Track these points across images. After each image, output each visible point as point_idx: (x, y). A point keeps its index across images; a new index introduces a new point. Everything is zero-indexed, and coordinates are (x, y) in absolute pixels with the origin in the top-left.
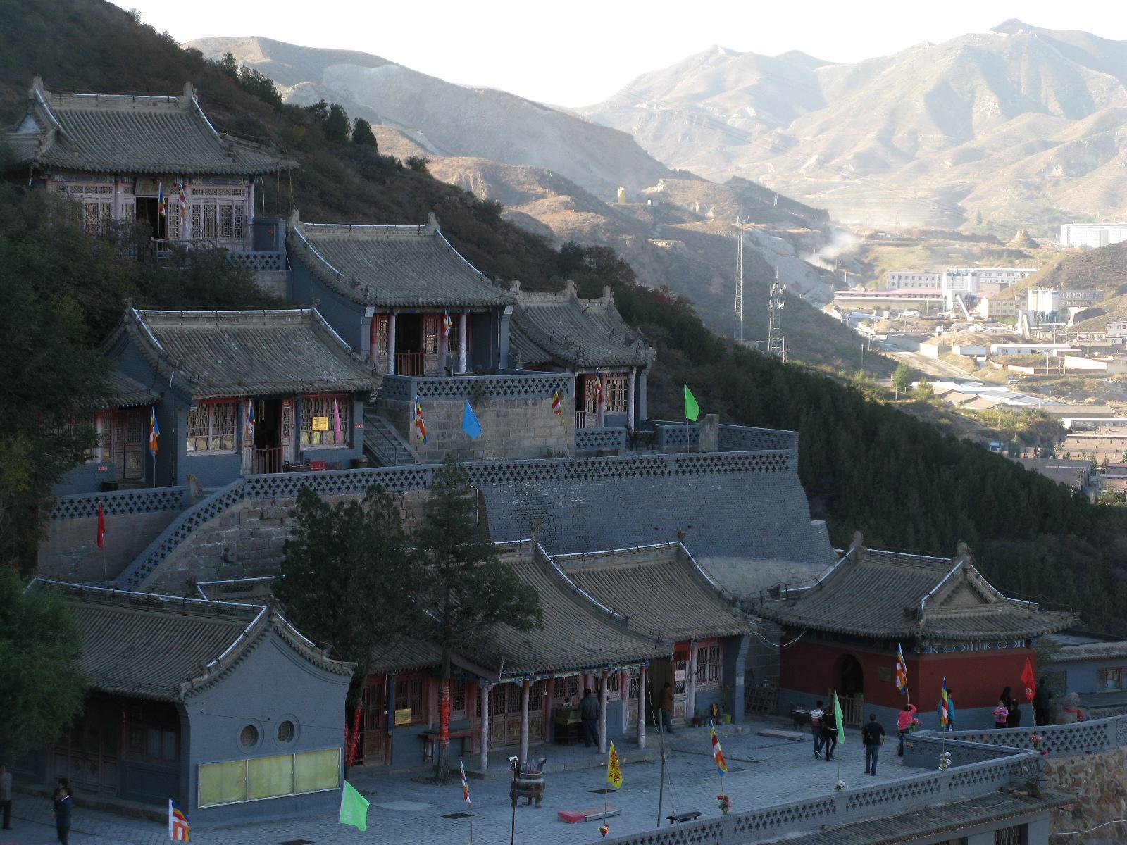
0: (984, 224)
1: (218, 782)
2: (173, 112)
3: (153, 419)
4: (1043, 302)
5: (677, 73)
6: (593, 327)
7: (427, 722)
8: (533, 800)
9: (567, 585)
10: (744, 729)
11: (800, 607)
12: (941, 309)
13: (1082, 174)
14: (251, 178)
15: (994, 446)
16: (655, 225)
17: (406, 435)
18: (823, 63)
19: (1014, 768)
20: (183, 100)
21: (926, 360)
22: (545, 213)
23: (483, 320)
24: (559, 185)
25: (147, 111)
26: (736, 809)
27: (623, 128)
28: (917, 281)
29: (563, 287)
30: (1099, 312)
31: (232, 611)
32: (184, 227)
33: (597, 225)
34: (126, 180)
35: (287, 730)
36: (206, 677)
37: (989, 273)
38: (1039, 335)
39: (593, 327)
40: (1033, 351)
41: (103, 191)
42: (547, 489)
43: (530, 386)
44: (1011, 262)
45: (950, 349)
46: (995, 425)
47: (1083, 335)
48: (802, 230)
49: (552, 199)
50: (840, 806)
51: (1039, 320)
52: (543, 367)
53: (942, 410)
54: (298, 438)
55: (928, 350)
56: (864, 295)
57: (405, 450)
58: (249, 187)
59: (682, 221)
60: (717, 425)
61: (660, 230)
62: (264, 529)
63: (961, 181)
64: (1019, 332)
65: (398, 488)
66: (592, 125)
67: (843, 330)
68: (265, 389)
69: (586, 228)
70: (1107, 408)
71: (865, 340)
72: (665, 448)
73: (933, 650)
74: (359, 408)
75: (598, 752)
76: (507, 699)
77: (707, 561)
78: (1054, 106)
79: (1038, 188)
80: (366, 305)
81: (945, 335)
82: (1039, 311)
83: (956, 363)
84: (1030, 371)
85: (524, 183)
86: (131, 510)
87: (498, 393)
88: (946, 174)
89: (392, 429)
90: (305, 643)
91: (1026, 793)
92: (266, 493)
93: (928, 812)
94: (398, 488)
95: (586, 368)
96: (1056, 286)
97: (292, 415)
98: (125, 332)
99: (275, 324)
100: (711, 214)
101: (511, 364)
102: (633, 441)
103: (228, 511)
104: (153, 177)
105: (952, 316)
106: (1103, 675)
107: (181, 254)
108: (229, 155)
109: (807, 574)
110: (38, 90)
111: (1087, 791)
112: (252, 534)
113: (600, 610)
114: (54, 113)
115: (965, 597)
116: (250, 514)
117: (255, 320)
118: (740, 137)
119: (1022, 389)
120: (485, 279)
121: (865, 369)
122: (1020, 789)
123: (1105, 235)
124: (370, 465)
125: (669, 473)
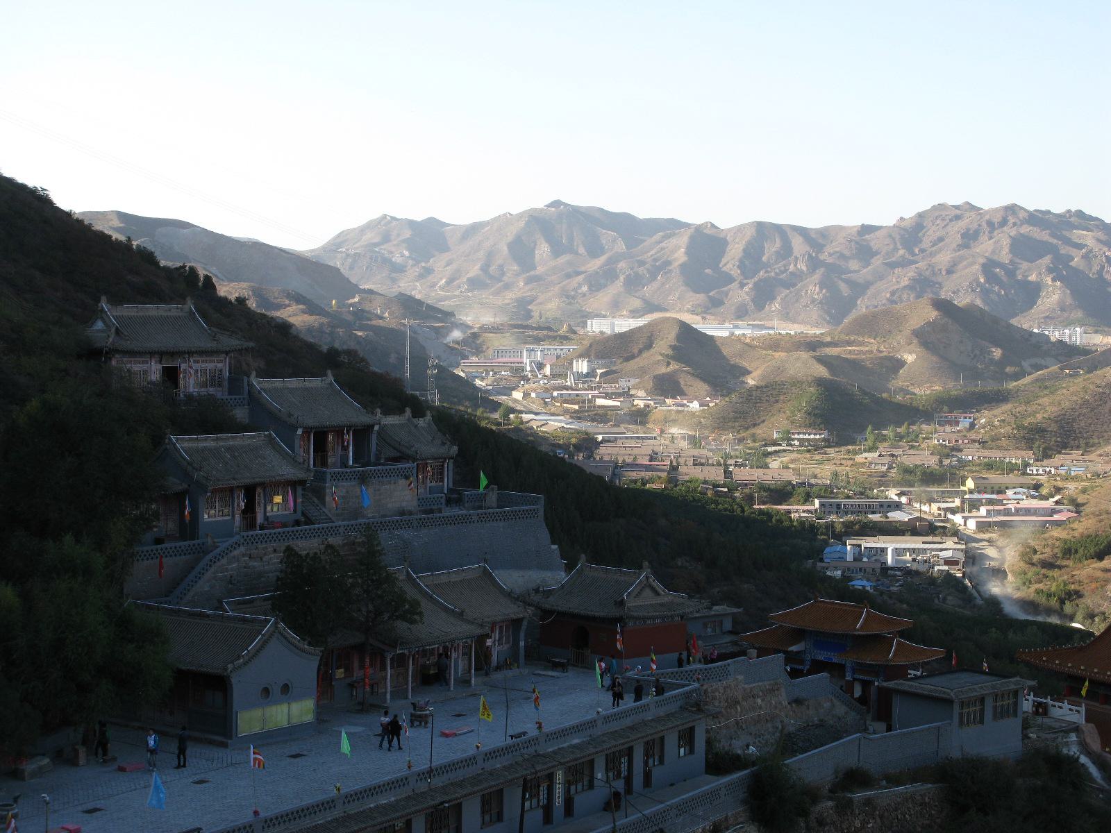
0: (543, 319)
1: (249, 720)
2: (181, 314)
3: (187, 502)
4: (582, 366)
5: (363, 230)
6: (423, 437)
7: (353, 676)
8: (423, 723)
9: (427, 593)
10: (525, 671)
11: (551, 599)
12: (523, 370)
13: (598, 290)
14: (227, 353)
15: (560, 453)
16: (355, 322)
17: (324, 503)
18: (449, 225)
19: (688, 695)
20: (186, 307)
21: (516, 401)
22: (290, 316)
23: (362, 433)
24: (299, 299)
25: (165, 314)
26: (546, 729)
27: (331, 264)
28: (508, 354)
29: (404, 412)
30: (615, 372)
31: (253, 621)
32: (189, 382)
33: (323, 323)
34: (156, 356)
35: (286, 689)
36: (242, 660)
37: (549, 349)
38: (580, 386)
39: (423, 437)
40: (577, 395)
41: (143, 362)
42: (407, 534)
43: (392, 473)
44: (561, 342)
45: (530, 394)
46: (559, 440)
47: (605, 386)
48: (440, 325)
49: (294, 308)
50: (599, 723)
51: (580, 377)
52: (395, 460)
53: (529, 431)
54: (265, 508)
55: (517, 395)
56: (478, 363)
57: (324, 512)
58: (225, 358)
59: (371, 320)
60: (496, 491)
61: (357, 325)
62: (252, 563)
63: (530, 294)
64: (569, 383)
65: (325, 536)
66: (315, 263)
67: (467, 384)
68: (248, 481)
69: (317, 325)
70: (622, 429)
71: (481, 390)
72: (466, 505)
73: (631, 624)
74: (300, 491)
75: (449, 690)
76: (400, 661)
77: (496, 572)
78: (582, 250)
79: (573, 298)
80: (297, 428)
81: (526, 386)
82: (580, 371)
83: (533, 403)
84: (576, 407)
85: (278, 298)
86: (176, 555)
87: (375, 477)
88: (521, 289)
89: (315, 500)
90: (295, 638)
91: (695, 709)
92: (252, 543)
93: (645, 723)
94: (325, 536)
95: (421, 460)
96: (589, 357)
97: (262, 495)
98: (166, 449)
99: (249, 441)
100: (387, 315)
101: (378, 458)
102: (449, 502)
103: (232, 554)
104: (173, 354)
105: (530, 374)
106: (705, 626)
107: (190, 397)
108: (215, 340)
109: (557, 577)
110: (104, 305)
111: (720, 702)
112: (245, 567)
113: (446, 607)
114: (113, 317)
115: (648, 592)
116: (244, 555)
117: (238, 440)
118: (399, 269)
119: (571, 417)
120: (362, 409)
121: (483, 407)
122: (692, 707)
123: (613, 325)
124: (306, 524)
125: (474, 522)
